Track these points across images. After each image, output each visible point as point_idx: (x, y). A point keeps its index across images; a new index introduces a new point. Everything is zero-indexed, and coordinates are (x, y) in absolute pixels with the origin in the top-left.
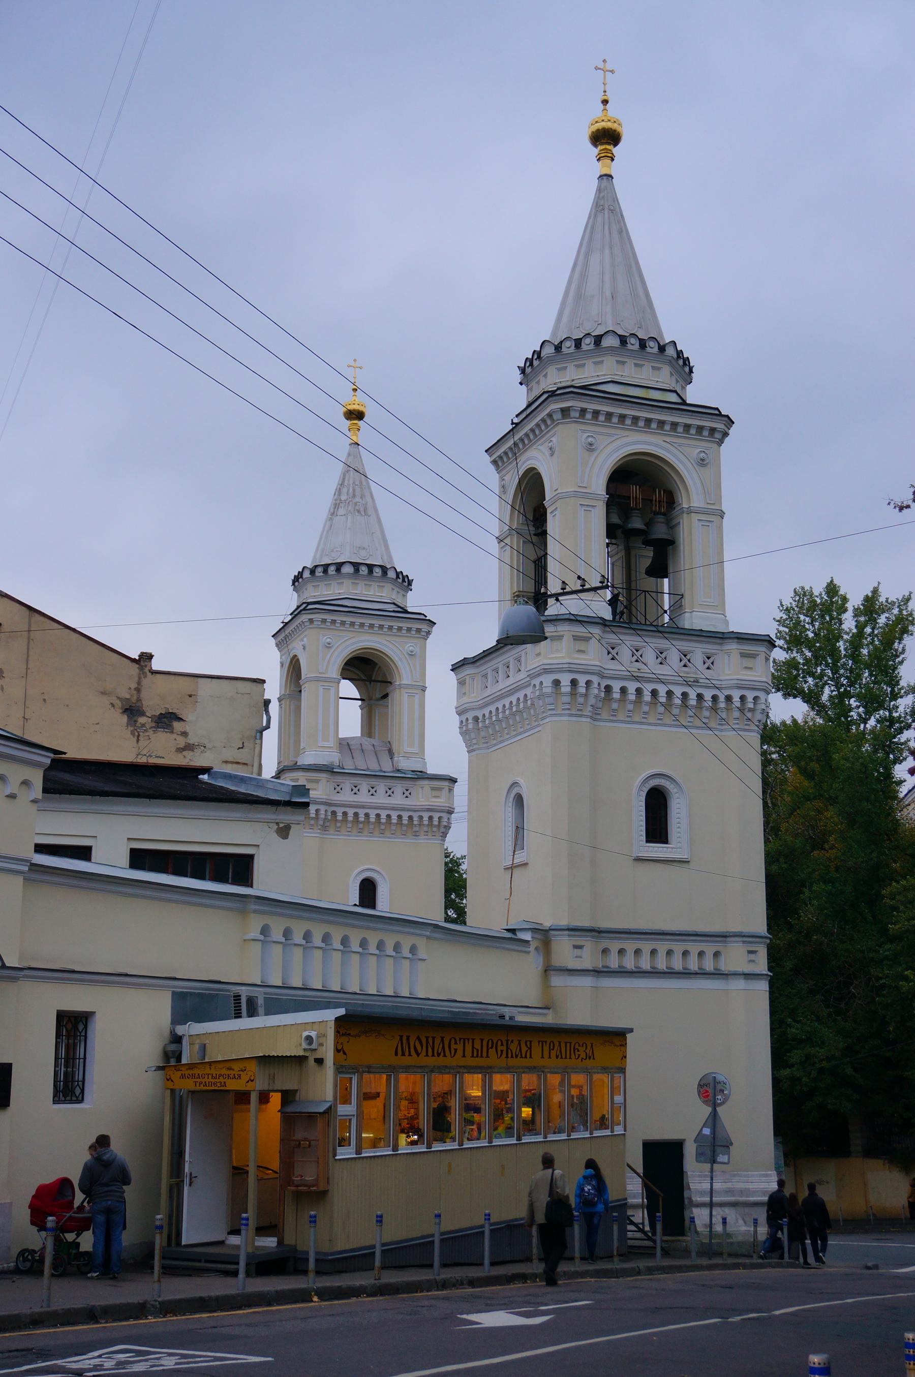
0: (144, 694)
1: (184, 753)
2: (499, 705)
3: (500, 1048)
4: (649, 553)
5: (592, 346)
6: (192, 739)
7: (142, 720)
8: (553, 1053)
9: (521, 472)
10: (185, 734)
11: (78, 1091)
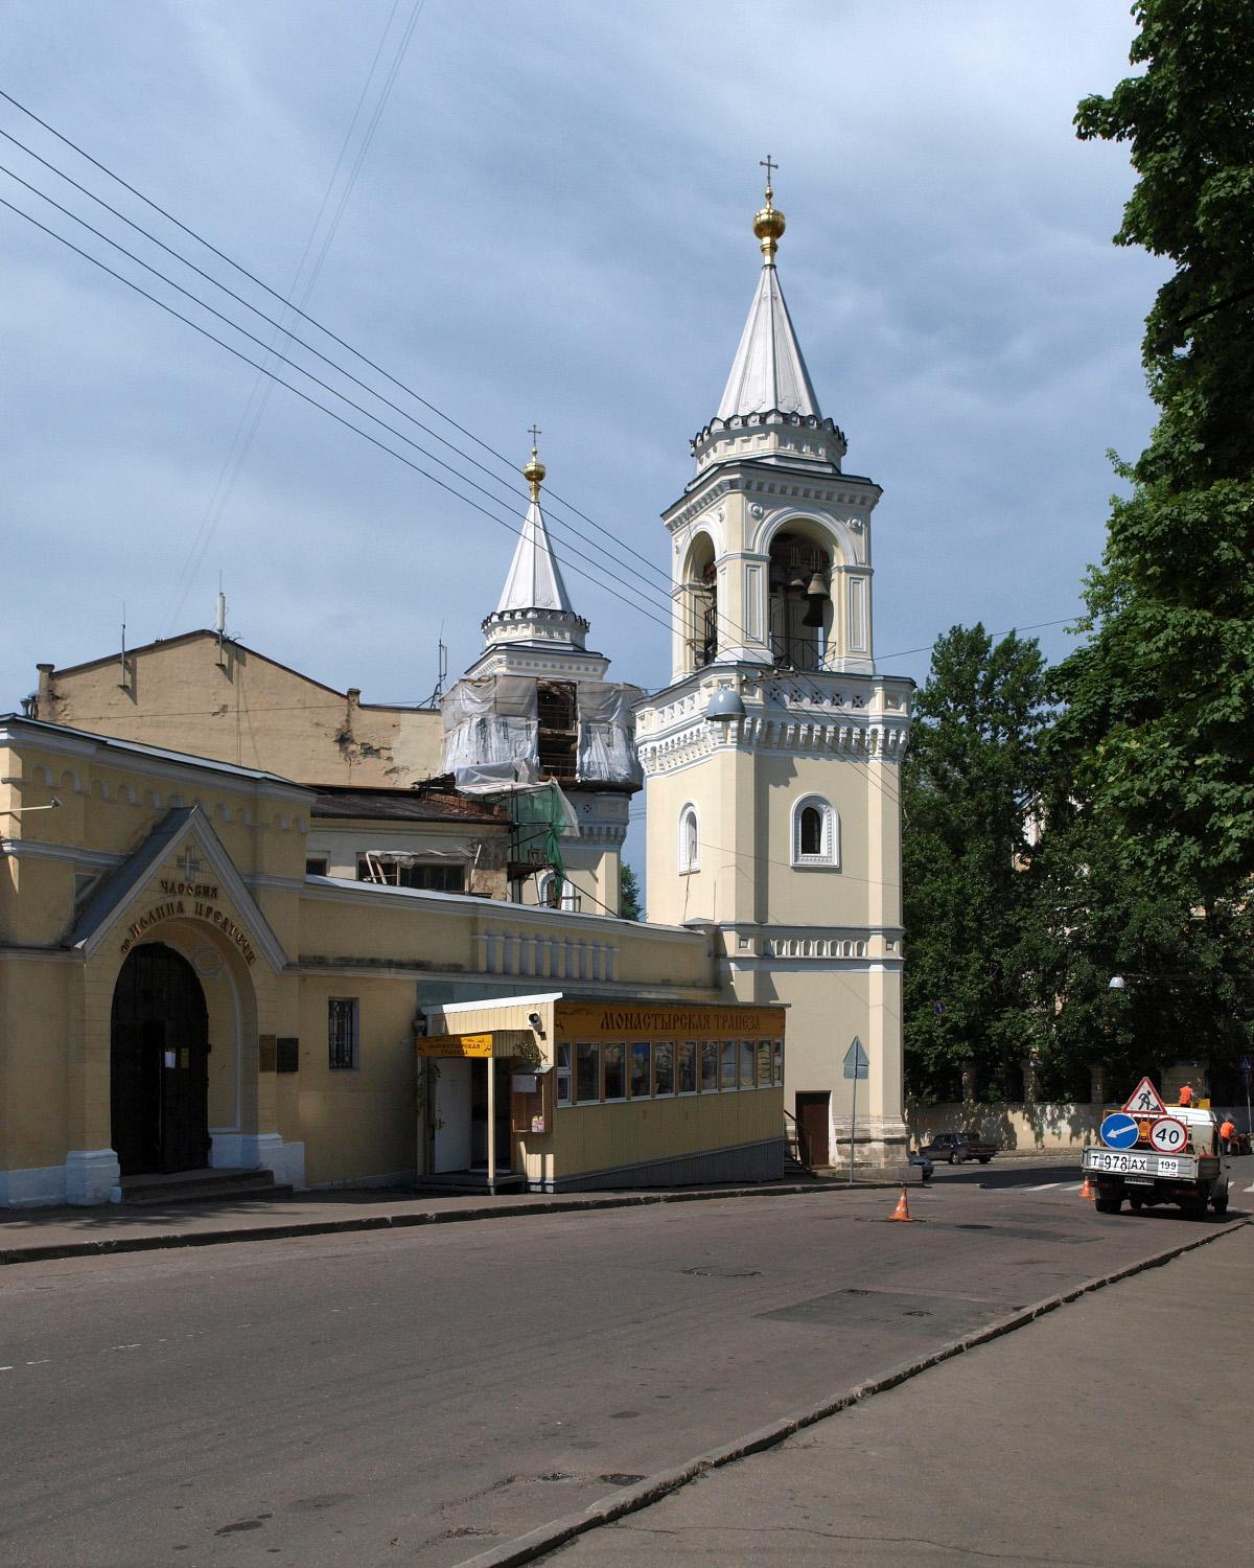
0: (354, 726)
1: (391, 775)
2: (675, 737)
3: (684, 1021)
4: (806, 605)
5: (758, 424)
6: (397, 762)
7: (352, 747)
8: (727, 1026)
9: (693, 535)
10: (390, 759)
11: (347, 1059)
